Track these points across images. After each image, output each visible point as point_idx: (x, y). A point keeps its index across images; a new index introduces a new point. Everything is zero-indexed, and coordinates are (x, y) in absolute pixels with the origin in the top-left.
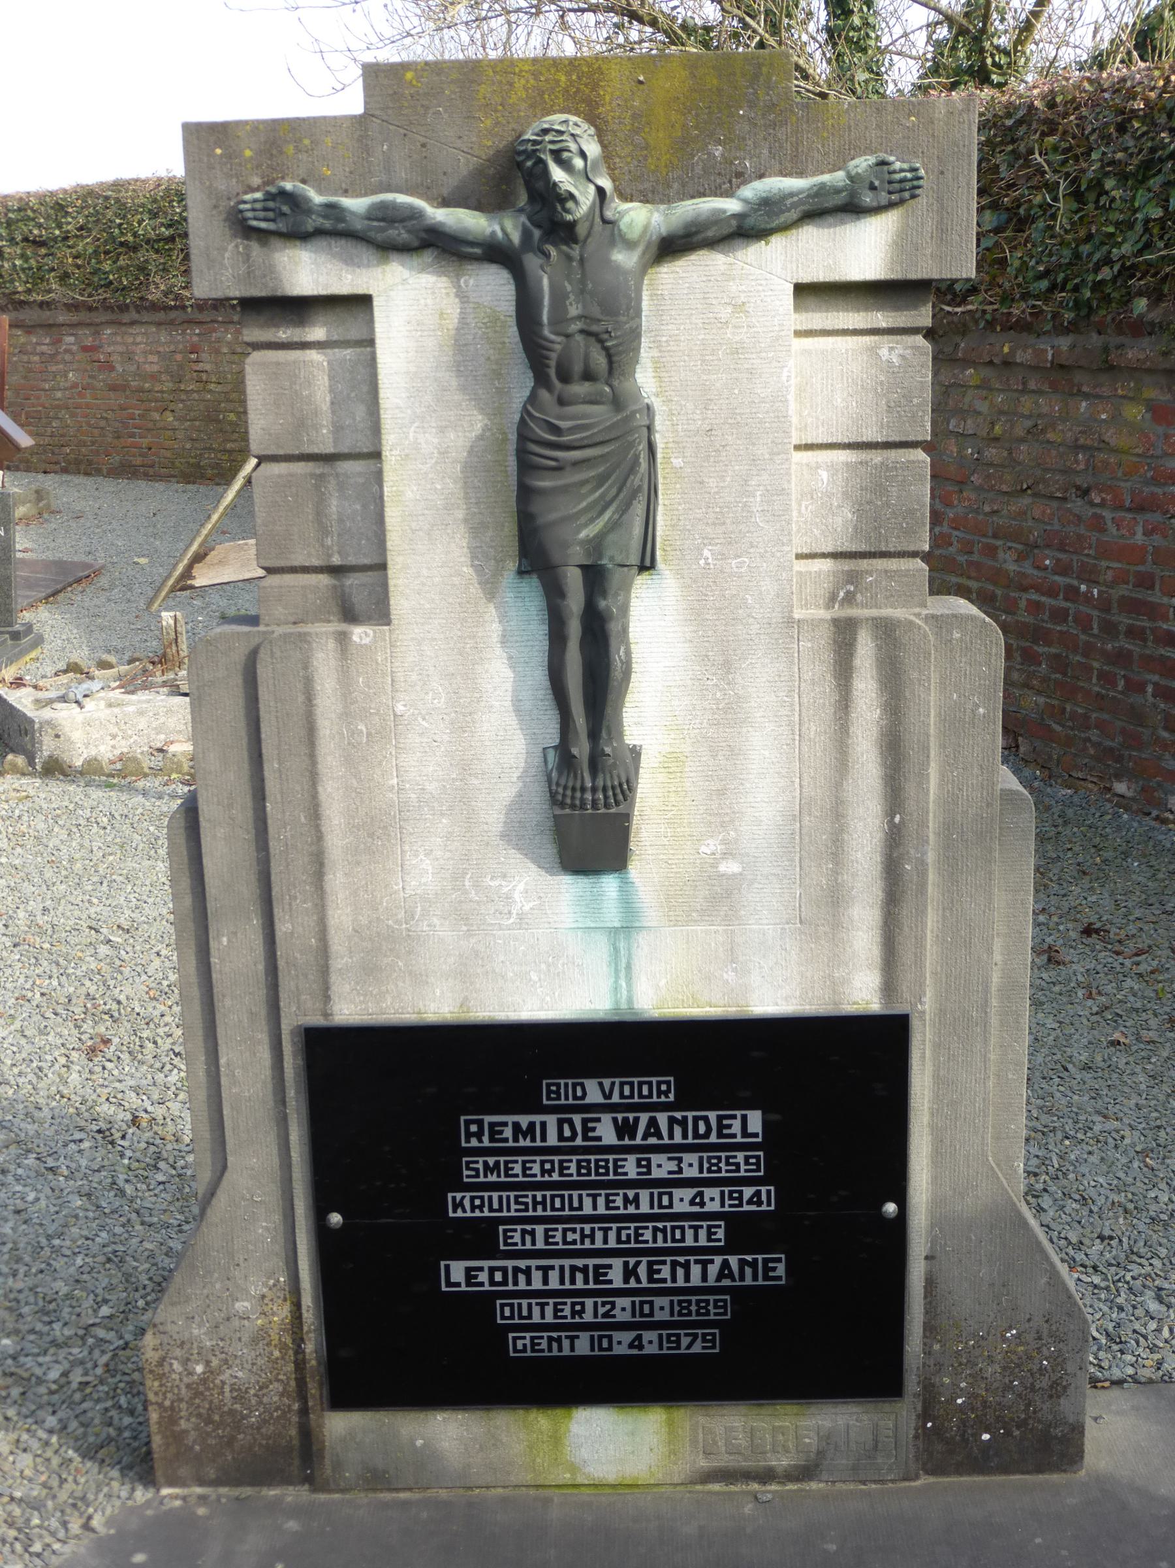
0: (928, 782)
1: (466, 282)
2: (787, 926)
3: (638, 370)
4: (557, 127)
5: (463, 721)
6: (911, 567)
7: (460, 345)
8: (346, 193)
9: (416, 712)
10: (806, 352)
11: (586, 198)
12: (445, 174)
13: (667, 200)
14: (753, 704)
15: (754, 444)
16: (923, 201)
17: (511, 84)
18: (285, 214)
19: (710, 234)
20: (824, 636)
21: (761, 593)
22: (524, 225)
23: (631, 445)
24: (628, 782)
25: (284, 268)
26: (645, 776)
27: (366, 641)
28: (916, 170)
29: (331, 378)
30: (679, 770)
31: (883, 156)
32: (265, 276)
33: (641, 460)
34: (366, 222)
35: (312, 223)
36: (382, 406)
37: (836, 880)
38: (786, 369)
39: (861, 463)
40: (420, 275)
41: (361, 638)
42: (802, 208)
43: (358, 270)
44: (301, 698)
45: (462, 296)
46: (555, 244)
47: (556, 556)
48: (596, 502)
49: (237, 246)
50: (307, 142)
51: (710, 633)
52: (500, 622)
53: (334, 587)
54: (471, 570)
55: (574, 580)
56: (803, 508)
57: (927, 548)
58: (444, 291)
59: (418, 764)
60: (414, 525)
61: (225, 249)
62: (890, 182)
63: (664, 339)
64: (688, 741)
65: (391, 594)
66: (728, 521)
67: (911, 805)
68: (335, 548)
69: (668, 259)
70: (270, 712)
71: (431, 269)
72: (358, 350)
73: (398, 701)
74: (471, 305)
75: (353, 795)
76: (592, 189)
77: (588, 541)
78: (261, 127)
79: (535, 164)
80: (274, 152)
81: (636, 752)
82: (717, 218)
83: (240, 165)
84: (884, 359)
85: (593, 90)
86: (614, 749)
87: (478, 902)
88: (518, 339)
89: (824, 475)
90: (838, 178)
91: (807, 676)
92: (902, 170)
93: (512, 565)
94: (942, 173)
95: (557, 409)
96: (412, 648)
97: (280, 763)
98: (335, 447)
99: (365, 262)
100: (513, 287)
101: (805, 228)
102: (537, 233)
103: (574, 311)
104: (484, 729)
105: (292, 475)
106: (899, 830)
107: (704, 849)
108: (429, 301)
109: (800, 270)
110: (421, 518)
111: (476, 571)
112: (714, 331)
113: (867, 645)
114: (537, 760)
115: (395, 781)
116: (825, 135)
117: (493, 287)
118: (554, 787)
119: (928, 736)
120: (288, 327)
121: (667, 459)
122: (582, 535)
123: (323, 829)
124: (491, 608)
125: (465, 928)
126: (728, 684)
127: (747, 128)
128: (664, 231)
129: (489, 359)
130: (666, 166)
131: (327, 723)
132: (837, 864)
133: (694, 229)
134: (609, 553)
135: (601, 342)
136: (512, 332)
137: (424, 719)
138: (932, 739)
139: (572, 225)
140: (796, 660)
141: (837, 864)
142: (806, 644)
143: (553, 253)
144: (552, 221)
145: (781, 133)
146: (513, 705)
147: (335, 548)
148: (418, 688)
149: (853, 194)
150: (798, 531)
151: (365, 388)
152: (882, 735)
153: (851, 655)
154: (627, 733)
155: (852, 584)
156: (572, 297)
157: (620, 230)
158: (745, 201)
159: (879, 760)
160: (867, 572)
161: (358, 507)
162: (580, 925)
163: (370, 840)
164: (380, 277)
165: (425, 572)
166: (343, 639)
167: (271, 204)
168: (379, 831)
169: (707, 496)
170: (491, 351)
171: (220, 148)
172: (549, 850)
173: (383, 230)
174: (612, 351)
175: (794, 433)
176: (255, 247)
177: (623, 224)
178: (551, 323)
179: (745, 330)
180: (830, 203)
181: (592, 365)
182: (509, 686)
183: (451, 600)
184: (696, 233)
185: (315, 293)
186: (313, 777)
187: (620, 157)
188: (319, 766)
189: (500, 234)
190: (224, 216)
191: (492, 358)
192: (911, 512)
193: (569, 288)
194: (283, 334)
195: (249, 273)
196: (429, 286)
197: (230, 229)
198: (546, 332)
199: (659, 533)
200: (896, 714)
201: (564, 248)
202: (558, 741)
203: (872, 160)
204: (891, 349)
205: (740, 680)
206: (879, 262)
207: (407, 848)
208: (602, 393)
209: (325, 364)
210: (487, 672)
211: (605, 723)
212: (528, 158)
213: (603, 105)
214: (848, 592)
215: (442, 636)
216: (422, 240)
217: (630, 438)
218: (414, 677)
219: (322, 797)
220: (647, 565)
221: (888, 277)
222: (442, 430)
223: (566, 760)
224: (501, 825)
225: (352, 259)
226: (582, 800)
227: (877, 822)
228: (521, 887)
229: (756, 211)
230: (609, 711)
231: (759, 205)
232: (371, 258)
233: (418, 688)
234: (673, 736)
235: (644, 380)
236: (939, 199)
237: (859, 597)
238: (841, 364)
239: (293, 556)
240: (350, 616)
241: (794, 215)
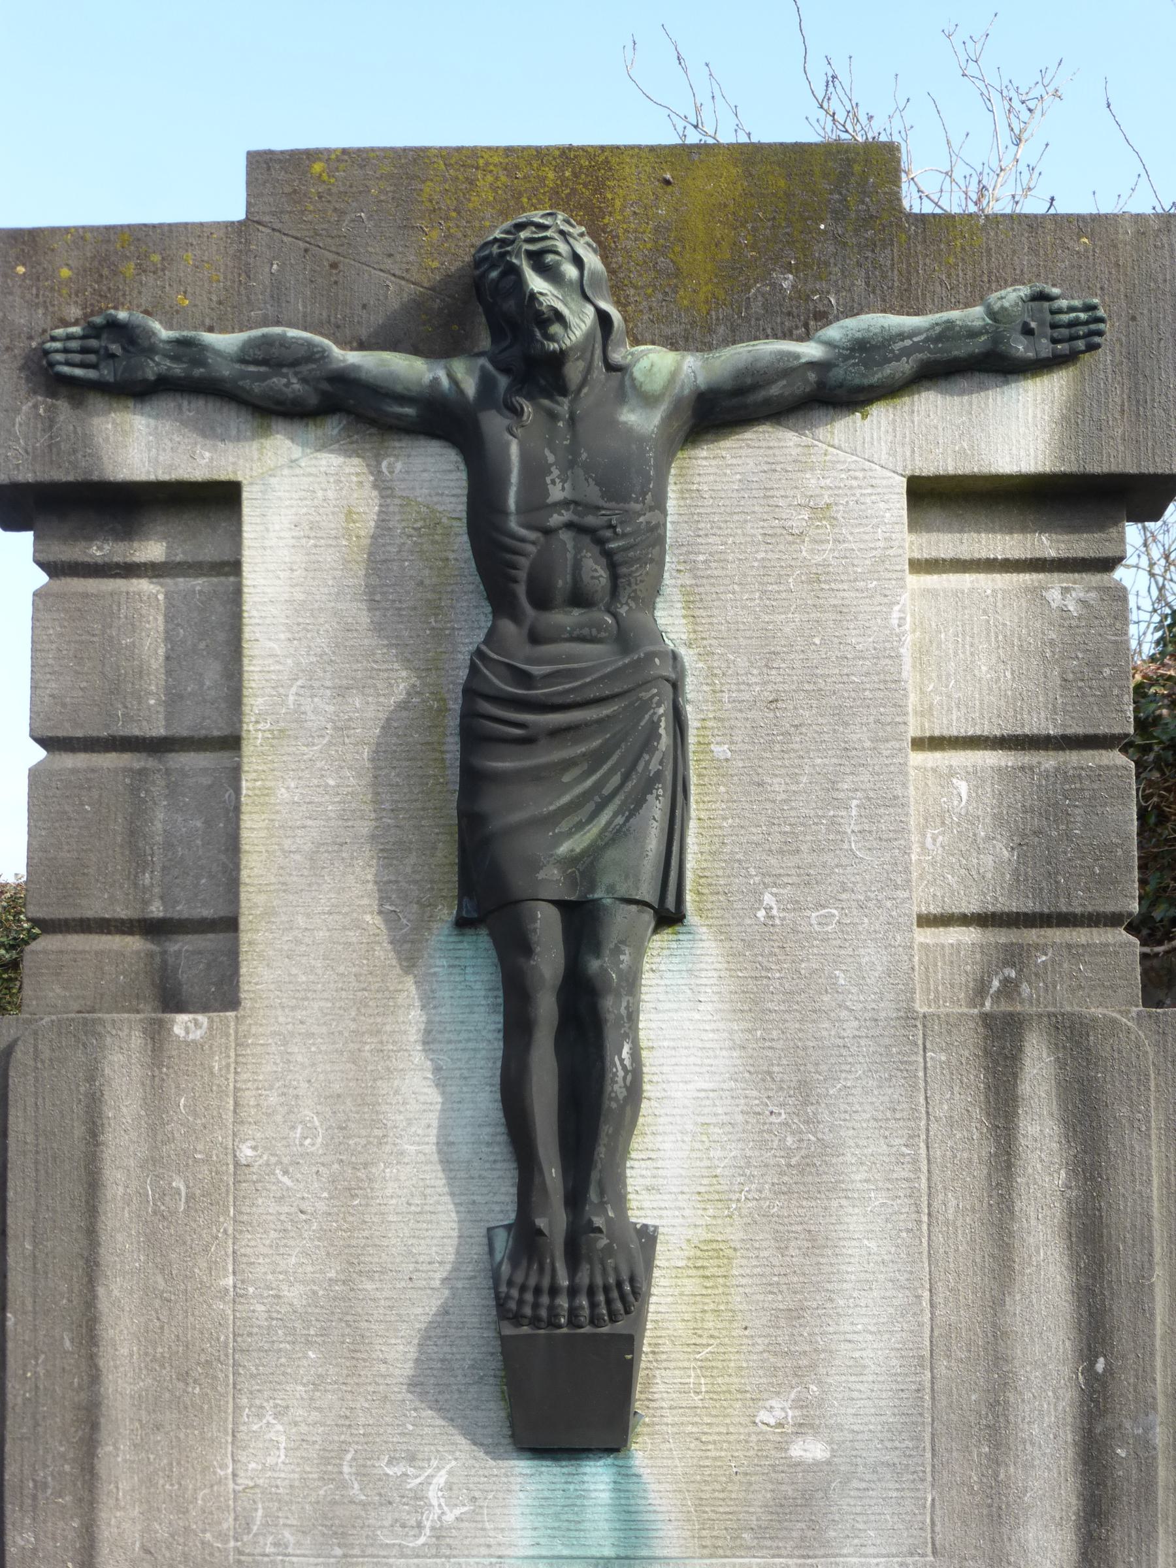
0: (1153, 1299)
1: (390, 465)
2: (909, 1560)
3: (659, 605)
5: (351, 1185)
6: (1111, 940)
7: (378, 563)
8: (211, 330)
9: (273, 1160)
10: (927, 592)
11: (580, 322)
12: (364, 306)
13: (710, 347)
14: (849, 1158)
15: (846, 724)
16: (1104, 357)
17: (472, 182)
18: (113, 356)
19: (774, 390)
20: (969, 1040)
21: (860, 968)
22: (483, 368)
23: (646, 705)
24: (632, 1280)
25: (107, 440)
26: (663, 1282)
27: (196, 1035)
28: (1094, 308)
29: (168, 619)
30: (721, 1272)
31: (1040, 286)
32: (75, 451)
33: (662, 731)
34: (237, 366)
35: (153, 368)
36: (246, 652)
37: (996, 1475)
38: (897, 608)
39: (1022, 768)
40: (318, 455)
41: (187, 1031)
42: (920, 356)
43: (221, 445)
44: (79, 1131)
45: (383, 486)
46: (530, 397)
47: (519, 884)
48: (586, 796)
49: (35, 406)
50: (156, 258)
51: (775, 1034)
52: (423, 1007)
53: (151, 955)
54: (378, 920)
55: (546, 925)
56: (929, 840)
57: (1135, 907)
58: (354, 479)
59: (274, 1264)
60: (287, 843)
61: (18, 411)
62: (1054, 326)
63: (701, 558)
64: (737, 1220)
65: (242, 957)
66: (804, 847)
67: (1123, 1341)
68: (156, 890)
69: (709, 437)
70: (24, 1153)
71: (336, 446)
72: (215, 580)
73: (244, 1141)
74: (397, 501)
75: (157, 1303)
76: (590, 310)
77: (572, 860)
78: (88, 236)
79: (504, 274)
80: (105, 272)
81: (648, 1237)
82: (788, 369)
83: (52, 289)
84: (1054, 605)
85: (595, 191)
86: (609, 1221)
87: (364, 1505)
88: (469, 554)
89: (963, 787)
90: (975, 315)
91: (941, 1111)
92: (1072, 309)
93: (446, 913)
94: (1134, 318)
95: (528, 650)
96: (273, 1049)
97: (35, 1244)
98: (166, 727)
99: (234, 432)
100: (464, 476)
101: (924, 395)
102: (503, 381)
103: (557, 493)
104: (389, 1192)
105: (93, 771)
106: (1104, 1385)
107: (763, 1416)
108: (331, 494)
109: (917, 457)
110: (299, 832)
111: (386, 921)
112: (781, 547)
113: (1040, 1059)
114: (476, 1249)
115: (230, 1281)
116: (952, 260)
117: (433, 474)
118: (503, 1289)
119: (1150, 1218)
120: (106, 540)
121: (704, 745)
122: (563, 849)
123: (101, 1363)
124: (409, 983)
125: (338, 1552)
126: (807, 1122)
127: (831, 249)
128: (702, 382)
129: (422, 583)
130: (707, 302)
131: (119, 1175)
132: (997, 1446)
133: (749, 381)
134: (606, 880)
135: (600, 542)
136: (461, 543)
137: (286, 1172)
138: (1156, 1225)
139: (559, 359)
140: (922, 1084)
141: (997, 1446)
142: (937, 1057)
143: (528, 408)
144: (530, 362)
145: (884, 257)
146: (439, 1152)
147: (156, 890)
148: (279, 1118)
149: (997, 339)
150: (921, 877)
151: (221, 636)
152: (1070, 1215)
153: (1015, 1076)
154: (633, 1204)
155: (1013, 965)
156: (556, 472)
157: (633, 379)
158: (829, 344)
159: (1066, 1260)
160: (1037, 947)
161: (199, 824)
162: (544, 1553)
163: (181, 1385)
164: (256, 455)
165: (301, 921)
166: (157, 1035)
167: (93, 343)
168: (199, 1382)
169: (769, 805)
170: (427, 572)
171: (24, 265)
172: (494, 1412)
173: (263, 377)
174: (617, 558)
175: (911, 719)
176: (63, 405)
177: (638, 372)
178: (519, 511)
179: (830, 546)
180: (962, 350)
181: (586, 578)
182: (433, 1118)
183: (341, 969)
184: (755, 387)
185: (152, 478)
186: (90, 1269)
187: (635, 287)
188: (102, 1251)
189: (445, 382)
190: (20, 362)
191: (427, 582)
192: (1109, 849)
193: (551, 459)
194: (98, 551)
195: (50, 446)
196: (332, 470)
197: (28, 380)
198: (513, 524)
199: (690, 865)
200: (1092, 1178)
201: (546, 402)
202: (513, 1216)
203: (1024, 291)
204: (1065, 591)
205: (826, 1117)
206: (1041, 446)
207: (244, 1401)
208: (599, 626)
209: (161, 597)
210: (397, 1092)
211: (595, 1176)
212: (493, 267)
213: (611, 214)
214: (1006, 981)
215: (324, 1030)
216: (324, 394)
217: (645, 695)
218: (273, 1099)
219: (104, 1305)
220: (669, 916)
221: (1056, 470)
222: (341, 692)
223: (525, 1237)
224: (411, 1364)
225: (213, 429)
226: (552, 1308)
227: (1066, 1371)
228: (441, 1479)
229: (846, 358)
230: (601, 1151)
231: (852, 350)
232: (243, 427)
233: (279, 1118)
234: (711, 1212)
235: (670, 620)
236: (1131, 356)
237: (1025, 989)
238: (985, 612)
239: (84, 902)
240: (172, 999)
241: (906, 366)
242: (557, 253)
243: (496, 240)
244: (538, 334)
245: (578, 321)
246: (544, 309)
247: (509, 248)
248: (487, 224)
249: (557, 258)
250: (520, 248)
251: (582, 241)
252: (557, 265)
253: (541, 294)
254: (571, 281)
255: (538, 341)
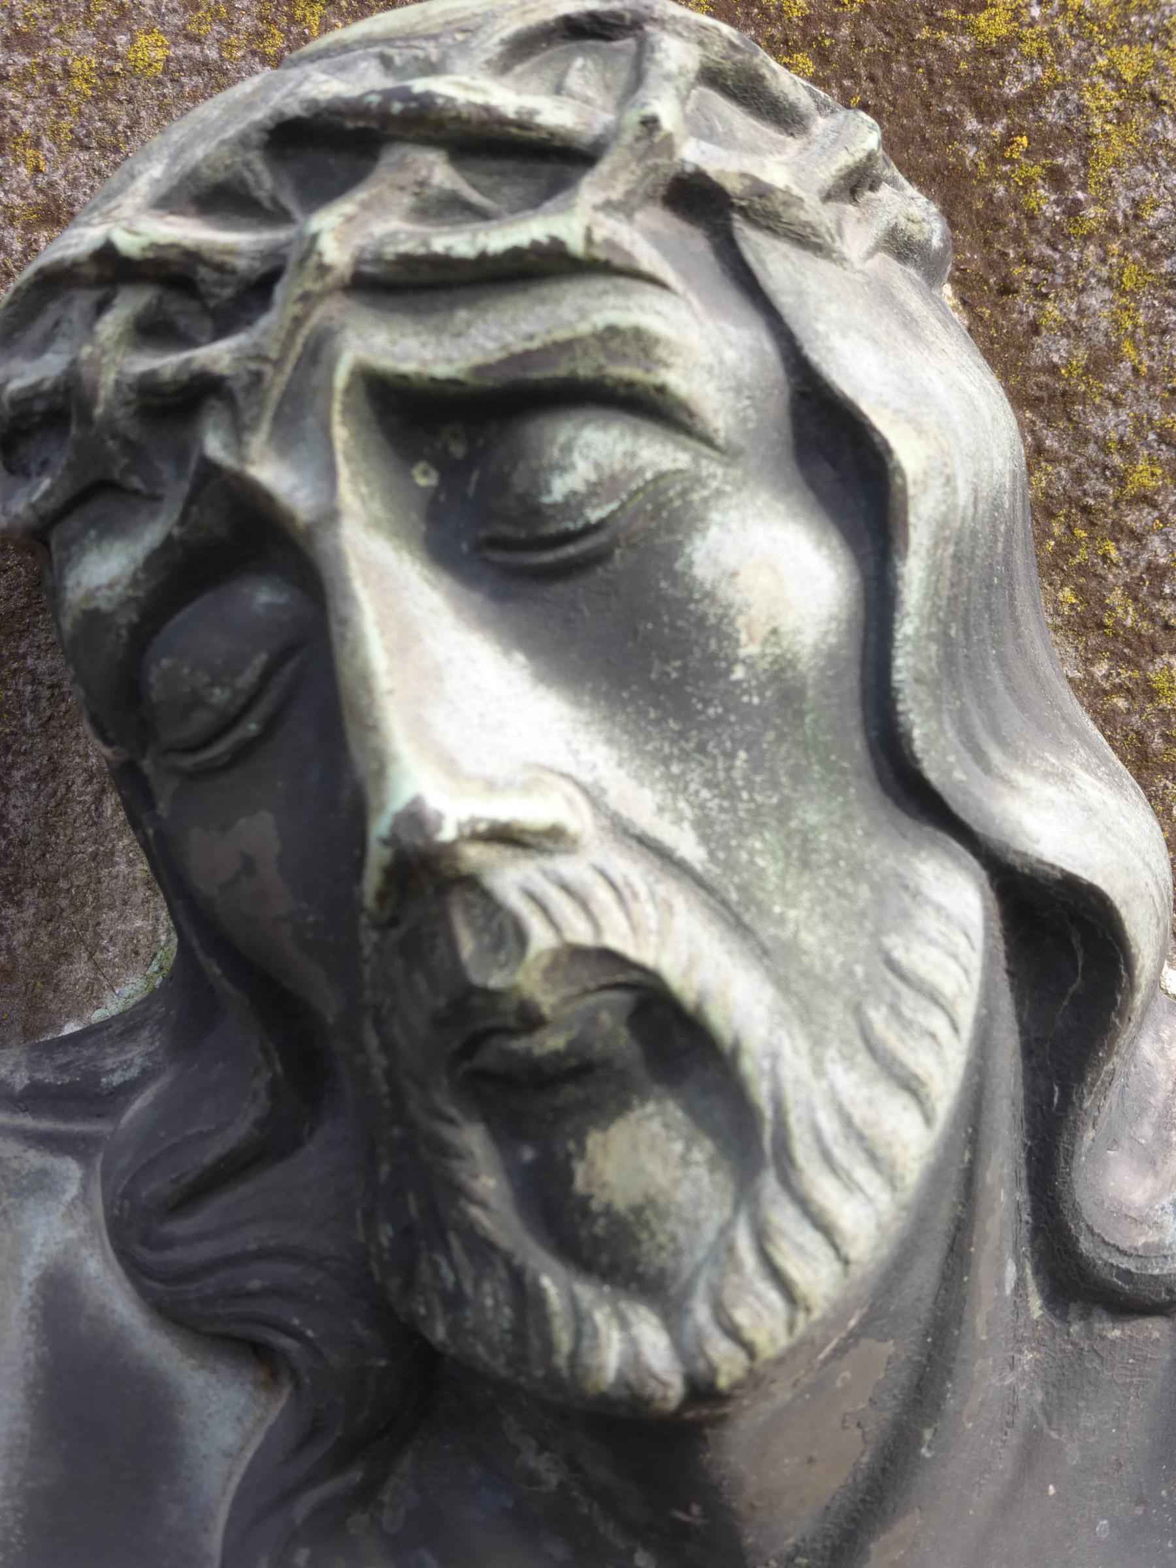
4: (471, 87)
22: (58, 1295)
79: (182, 577)
102: (224, 1420)
212: (98, 497)
242: (654, 408)
243: (111, 269)
244: (487, 1182)
245: (852, 1082)
246: (529, 979)
247: (218, 355)
248: (152, 50)
249: (658, 453)
250: (318, 352)
251: (857, 232)
252: (658, 521)
253: (506, 836)
254: (781, 677)
255: (482, 1248)
